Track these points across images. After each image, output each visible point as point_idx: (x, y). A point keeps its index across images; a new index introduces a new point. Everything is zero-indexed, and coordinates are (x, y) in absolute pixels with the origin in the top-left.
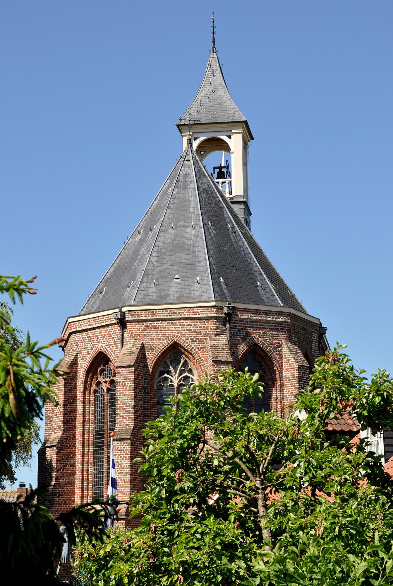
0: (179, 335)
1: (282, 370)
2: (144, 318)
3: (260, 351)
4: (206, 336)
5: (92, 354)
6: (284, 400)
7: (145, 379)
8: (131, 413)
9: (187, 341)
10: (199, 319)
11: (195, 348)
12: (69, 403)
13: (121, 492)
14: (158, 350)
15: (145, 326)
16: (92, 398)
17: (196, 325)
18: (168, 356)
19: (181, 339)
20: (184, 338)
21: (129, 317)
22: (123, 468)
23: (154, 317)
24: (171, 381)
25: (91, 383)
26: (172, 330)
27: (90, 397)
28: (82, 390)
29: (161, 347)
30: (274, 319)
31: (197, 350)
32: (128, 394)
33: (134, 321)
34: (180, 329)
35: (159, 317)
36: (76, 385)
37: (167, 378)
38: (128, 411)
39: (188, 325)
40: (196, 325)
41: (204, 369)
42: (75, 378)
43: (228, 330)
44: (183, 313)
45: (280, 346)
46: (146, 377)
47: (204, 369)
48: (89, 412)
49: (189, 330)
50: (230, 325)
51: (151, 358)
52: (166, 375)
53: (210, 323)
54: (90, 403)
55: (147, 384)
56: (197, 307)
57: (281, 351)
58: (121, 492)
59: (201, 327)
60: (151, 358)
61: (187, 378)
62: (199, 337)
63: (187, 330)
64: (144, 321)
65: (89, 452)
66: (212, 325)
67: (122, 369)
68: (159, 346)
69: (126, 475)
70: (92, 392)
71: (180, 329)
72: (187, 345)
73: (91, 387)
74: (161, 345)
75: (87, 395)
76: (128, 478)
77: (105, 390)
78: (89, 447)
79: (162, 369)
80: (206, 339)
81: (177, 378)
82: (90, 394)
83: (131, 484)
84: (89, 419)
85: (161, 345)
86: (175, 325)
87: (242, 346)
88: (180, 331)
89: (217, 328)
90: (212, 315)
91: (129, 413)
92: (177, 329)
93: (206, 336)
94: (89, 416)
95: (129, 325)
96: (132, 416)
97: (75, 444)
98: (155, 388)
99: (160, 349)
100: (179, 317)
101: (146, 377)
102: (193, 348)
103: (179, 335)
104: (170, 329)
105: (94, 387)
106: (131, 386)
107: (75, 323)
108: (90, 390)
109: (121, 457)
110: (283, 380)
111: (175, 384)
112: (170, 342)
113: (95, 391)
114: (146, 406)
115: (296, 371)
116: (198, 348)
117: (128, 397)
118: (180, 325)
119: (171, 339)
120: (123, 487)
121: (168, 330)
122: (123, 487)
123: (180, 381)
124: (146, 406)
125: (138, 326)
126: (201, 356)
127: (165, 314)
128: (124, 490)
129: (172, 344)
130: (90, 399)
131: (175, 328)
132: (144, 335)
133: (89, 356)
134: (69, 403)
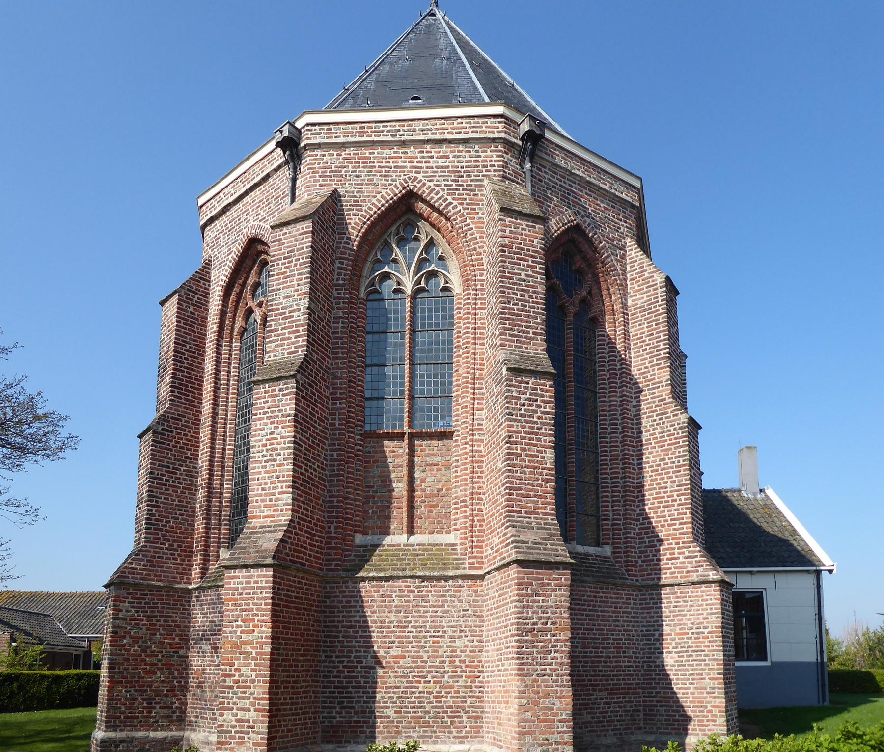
0: (420, 176)
1: (624, 295)
2: (342, 140)
3: (585, 247)
4: (481, 180)
5: (237, 248)
6: (630, 353)
7: (339, 268)
8: (302, 325)
9: (437, 189)
10: (465, 141)
11: (455, 203)
12: (186, 350)
13: (270, 506)
14: (370, 209)
15: (344, 159)
16: (236, 345)
17: (459, 156)
18: (394, 229)
19: (424, 184)
20: (431, 184)
21: (308, 138)
22: (275, 449)
23: (365, 139)
24: (399, 284)
25: (235, 316)
26: (405, 167)
27: (231, 342)
28: (215, 328)
29: (379, 201)
30: (613, 191)
31: (460, 207)
32: (295, 282)
33: (319, 146)
34: (424, 165)
35: (376, 139)
36: (204, 320)
37: (386, 276)
38: (293, 322)
39: (441, 157)
40: (459, 156)
41: (475, 249)
42: (203, 306)
43: (528, 175)
44: (430, 130)
45: (623, 248)
46: (342, 263)
47: (475, 249)
48: (229, 372)
49: (442, 167)
50: (532, 166)
51: (355, 223)
52: (386, 269)
53: (489, 153)
54: (230, 355)
55: (344, 280)
56: (462, 117)
57: (623, 257)
58: (270, 506)
59: (470, 161)
60: (355, 223)
61: (433, 274)
62: (465, 181)
63: (437, 167)
64: (343, 146)
65: (224, 449)
66: (495, 158)
67: (285, 230)
68: (374, 200)
69: (282, 465)
70: (236, 330)
71: (424, 165)
72: (436, 197)
73: (234, 323)
74: (379, 196)
75: (226, 338)
76: (288, 470)
77: (259, 320)
78: (225, 441)
79: (379, 257)
80: (481, 186)
81: (411, 274)
82: (231, 338)
83: (293, 487)
84: (228, 385)
85: (379, 196)
86: (411, 157)
87: (554, 221)
88: (421, 168)
89: (505, 166)
90: (496, 135)
91: (297, 326)
92: (415, 164)
93: (481, 180)
94: (229, 381)
95: (307, 159)
96: (303, 331)
97: (199, 433)
98: (362, 295)
99: (376, 206)
100: (422, 137)
101: (342, 263)
102: (451, 203)
103: (420, 176)
104: (400, 164)
105: (239, 323)
106: (305, 263)
107: (208, 204)
108: (232, 330)
109: (272, 423)
110: (627, 314)
111: (408, 287)
112: (326, 192)
113: (244, 330)
114: (340, 325)
115: (659, 290)
116: (462, 204)
117: (297, 290)
118: (423, 157)
119: (401, 184)
120: (274, 494)
121: (396, 167)
122: (274, 494)
123: (418, 282)
124: (340, 325)
125: (332, 158)
126: (468, 221)
127: (388, 131)
128: (277, 500)
129: (403, 196)
130: (231, 346)
131: (410, 162)
132: (341, 176)
133: (230, 257)
134: (186, 350)
